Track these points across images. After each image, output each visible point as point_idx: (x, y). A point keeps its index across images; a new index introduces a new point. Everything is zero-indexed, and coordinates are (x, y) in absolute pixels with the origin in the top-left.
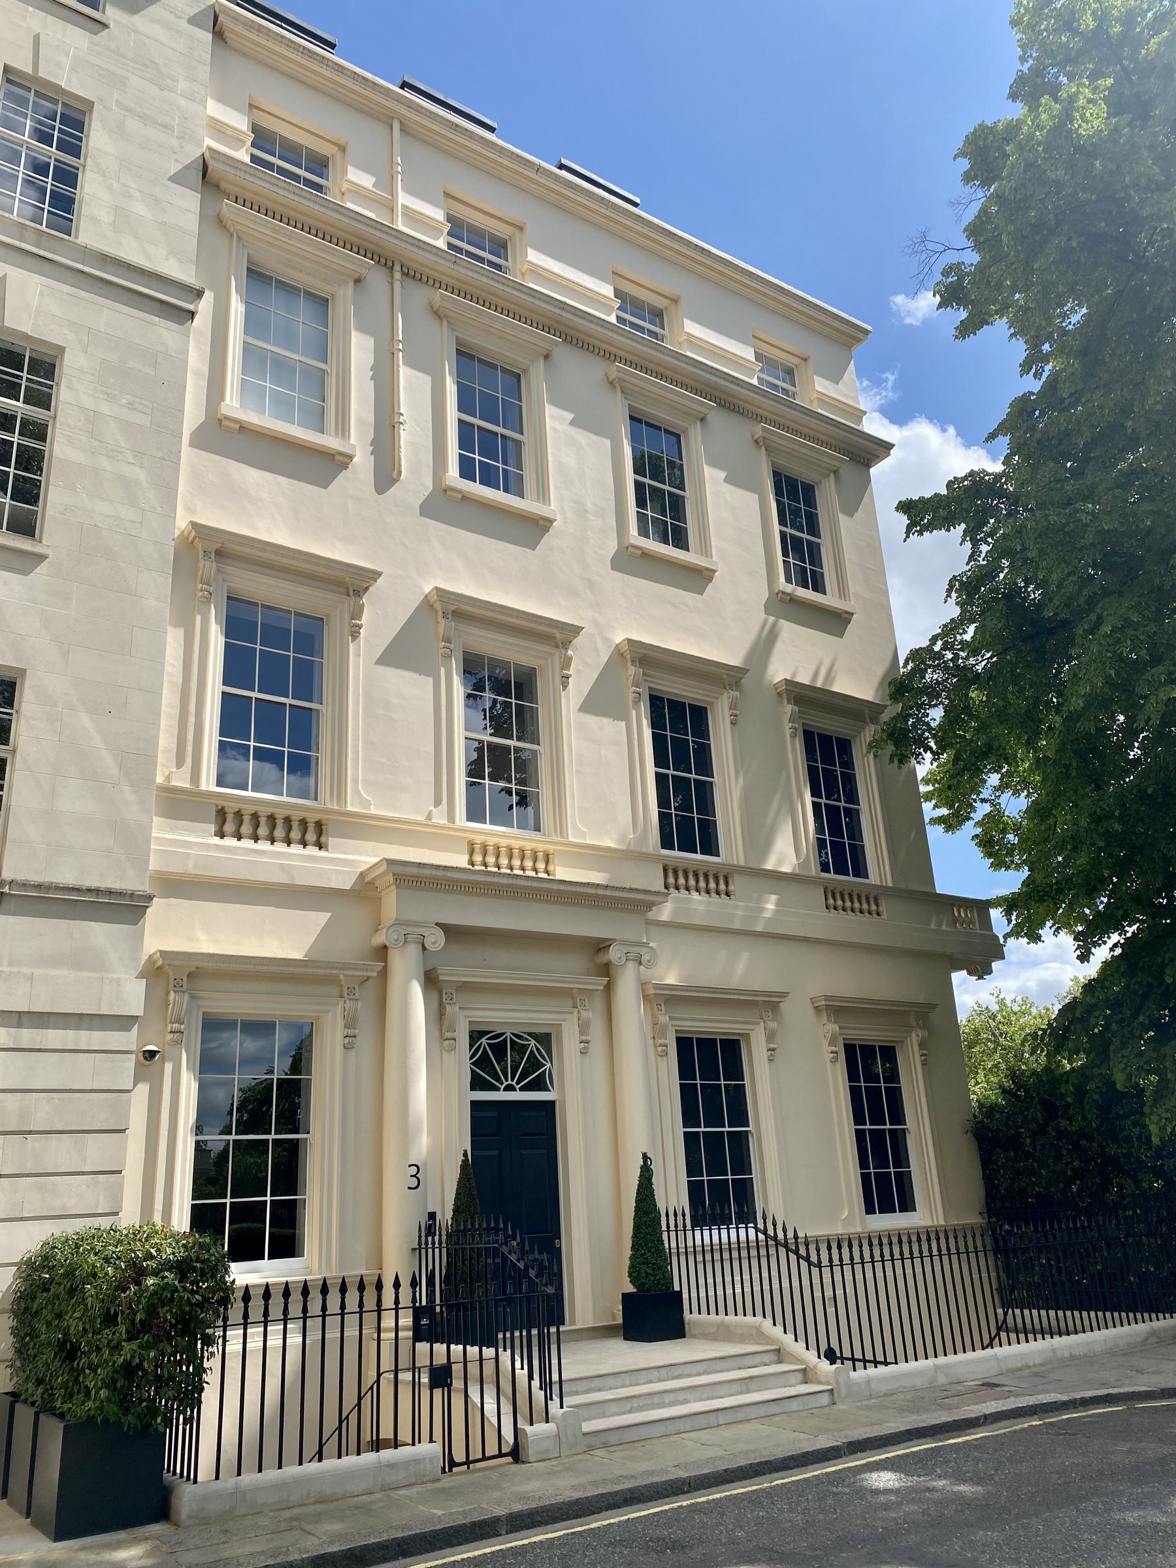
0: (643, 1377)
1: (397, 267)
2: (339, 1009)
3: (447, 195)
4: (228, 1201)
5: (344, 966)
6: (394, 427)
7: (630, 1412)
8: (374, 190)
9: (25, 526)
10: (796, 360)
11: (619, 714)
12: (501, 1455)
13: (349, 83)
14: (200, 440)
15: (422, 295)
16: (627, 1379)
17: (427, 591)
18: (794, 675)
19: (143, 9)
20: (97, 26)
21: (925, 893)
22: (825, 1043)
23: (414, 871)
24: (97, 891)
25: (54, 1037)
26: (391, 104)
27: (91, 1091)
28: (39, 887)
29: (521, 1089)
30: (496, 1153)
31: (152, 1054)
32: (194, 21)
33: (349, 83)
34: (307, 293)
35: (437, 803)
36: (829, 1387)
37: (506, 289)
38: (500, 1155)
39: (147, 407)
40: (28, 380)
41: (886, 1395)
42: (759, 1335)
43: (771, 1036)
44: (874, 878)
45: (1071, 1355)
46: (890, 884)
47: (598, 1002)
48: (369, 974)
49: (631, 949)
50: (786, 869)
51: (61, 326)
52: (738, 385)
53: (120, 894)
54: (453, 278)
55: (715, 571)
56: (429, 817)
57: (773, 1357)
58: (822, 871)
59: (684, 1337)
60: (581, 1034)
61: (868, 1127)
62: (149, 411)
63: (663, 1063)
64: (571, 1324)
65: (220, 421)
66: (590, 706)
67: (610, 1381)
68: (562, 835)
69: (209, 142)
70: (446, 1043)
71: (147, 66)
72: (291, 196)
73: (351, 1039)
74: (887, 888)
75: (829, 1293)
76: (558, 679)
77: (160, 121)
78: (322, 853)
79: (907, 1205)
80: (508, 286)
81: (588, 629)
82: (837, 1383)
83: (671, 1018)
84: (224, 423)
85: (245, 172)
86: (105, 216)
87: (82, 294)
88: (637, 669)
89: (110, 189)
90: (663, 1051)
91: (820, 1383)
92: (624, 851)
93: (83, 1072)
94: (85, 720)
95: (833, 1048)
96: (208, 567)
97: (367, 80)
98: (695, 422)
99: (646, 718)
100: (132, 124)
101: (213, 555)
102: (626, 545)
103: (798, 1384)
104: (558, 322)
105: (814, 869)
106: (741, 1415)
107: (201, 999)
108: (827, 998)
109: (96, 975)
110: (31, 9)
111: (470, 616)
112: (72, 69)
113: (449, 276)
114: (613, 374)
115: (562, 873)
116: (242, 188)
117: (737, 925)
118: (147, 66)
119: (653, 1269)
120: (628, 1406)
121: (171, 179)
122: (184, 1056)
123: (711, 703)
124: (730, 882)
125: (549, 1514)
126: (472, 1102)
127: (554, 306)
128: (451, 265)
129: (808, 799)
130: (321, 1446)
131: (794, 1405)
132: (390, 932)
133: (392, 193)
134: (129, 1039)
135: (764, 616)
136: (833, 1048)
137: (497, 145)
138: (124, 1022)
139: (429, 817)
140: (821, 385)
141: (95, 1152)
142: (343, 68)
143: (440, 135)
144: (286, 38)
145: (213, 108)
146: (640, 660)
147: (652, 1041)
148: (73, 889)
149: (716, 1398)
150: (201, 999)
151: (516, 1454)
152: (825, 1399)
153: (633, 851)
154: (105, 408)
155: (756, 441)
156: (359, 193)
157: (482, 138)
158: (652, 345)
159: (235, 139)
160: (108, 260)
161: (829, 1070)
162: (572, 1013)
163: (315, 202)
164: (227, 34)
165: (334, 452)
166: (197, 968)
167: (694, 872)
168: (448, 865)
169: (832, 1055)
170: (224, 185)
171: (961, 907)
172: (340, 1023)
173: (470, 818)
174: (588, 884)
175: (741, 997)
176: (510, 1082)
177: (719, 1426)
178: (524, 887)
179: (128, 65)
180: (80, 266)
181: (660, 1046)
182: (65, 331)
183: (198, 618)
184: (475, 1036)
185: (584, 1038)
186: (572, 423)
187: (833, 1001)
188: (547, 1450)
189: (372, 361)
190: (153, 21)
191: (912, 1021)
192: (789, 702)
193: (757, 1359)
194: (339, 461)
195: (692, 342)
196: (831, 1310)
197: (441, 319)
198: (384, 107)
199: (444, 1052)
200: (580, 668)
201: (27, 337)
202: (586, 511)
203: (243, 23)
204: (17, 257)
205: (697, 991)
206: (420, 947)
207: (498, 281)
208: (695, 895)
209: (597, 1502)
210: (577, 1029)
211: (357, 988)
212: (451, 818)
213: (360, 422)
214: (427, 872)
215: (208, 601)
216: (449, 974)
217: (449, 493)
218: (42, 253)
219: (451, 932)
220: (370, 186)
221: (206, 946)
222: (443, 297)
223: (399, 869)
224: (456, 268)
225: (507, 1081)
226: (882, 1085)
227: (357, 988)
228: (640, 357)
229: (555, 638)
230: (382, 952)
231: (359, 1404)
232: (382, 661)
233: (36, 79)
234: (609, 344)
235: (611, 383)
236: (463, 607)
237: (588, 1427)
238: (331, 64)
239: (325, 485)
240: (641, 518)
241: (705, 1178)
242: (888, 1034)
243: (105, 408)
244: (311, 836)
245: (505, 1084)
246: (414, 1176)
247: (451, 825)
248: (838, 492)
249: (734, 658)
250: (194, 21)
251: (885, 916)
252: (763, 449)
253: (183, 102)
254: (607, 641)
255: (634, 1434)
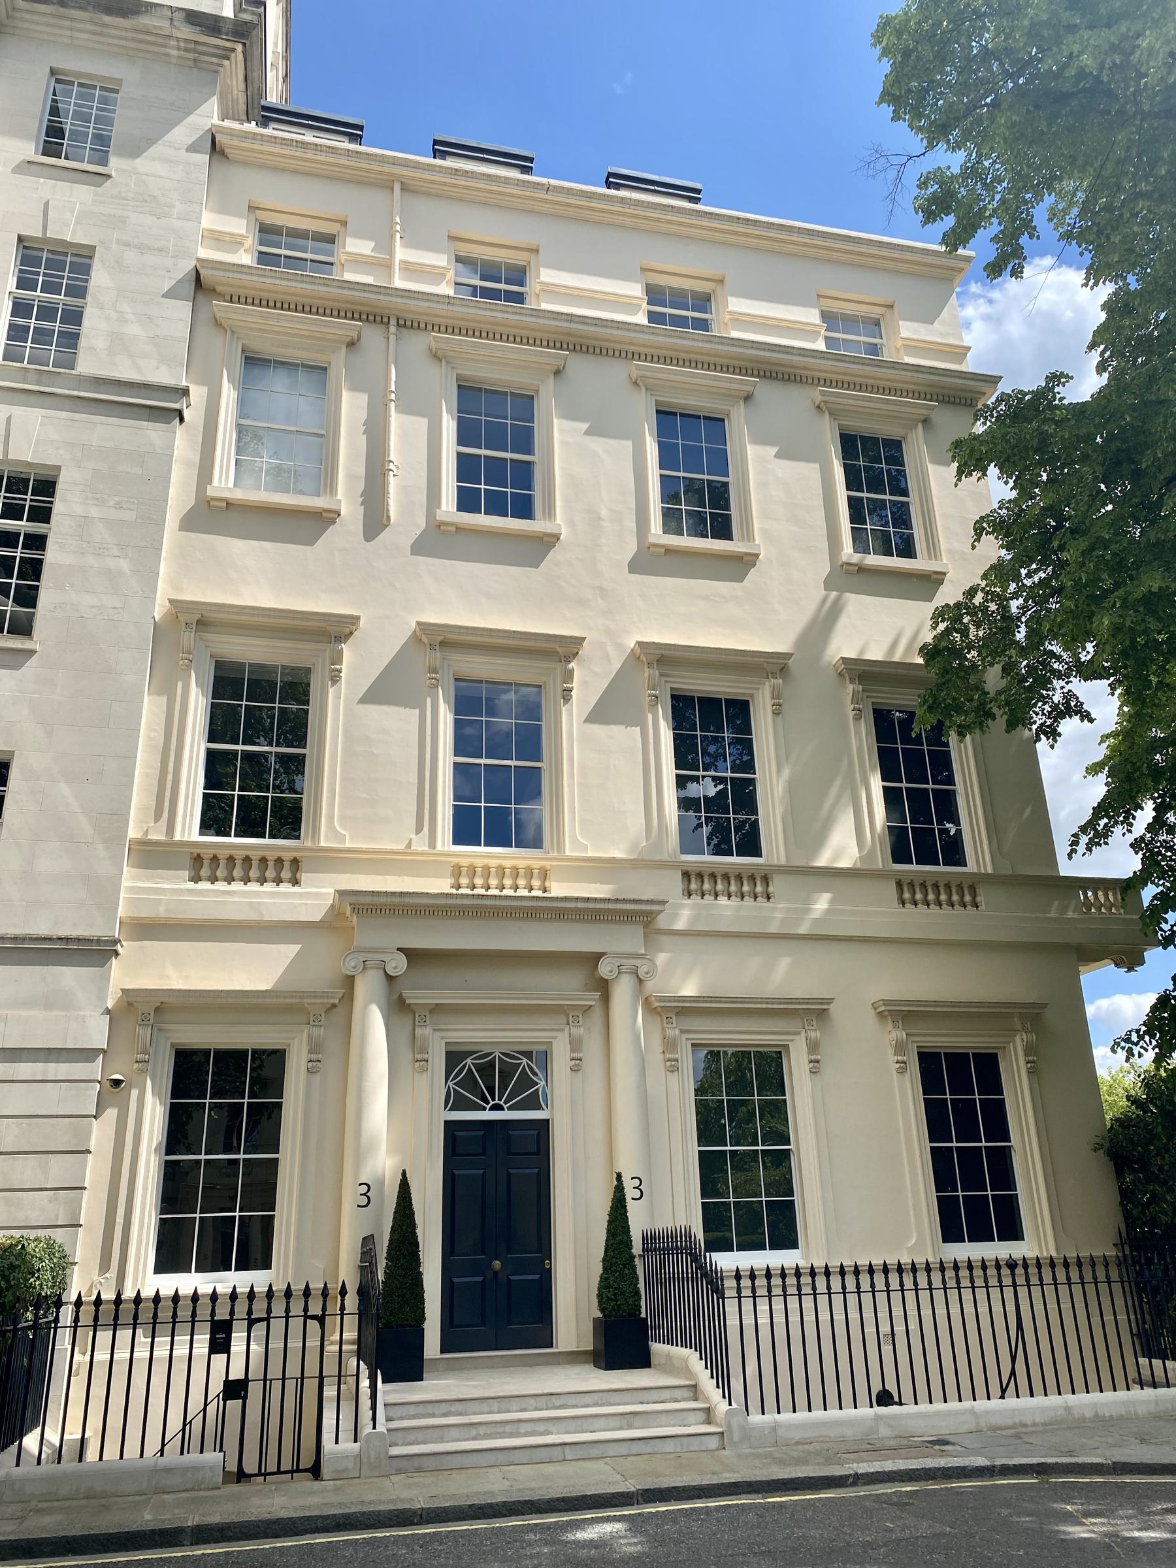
0: (514, 1404)
1: (393, 321)
2: (305, 1036)
3: (452, 238)
4: (237, 1214)
5: (315, 995)
6: (384, 473)
7: (474, 1439)
8: (373, 254)
9: (22, 628)
10: (880, 310)
11: (631, 718)
12: (279, 1472)
13: (343, 161)
14: (190, 523)
15: (418, 343)
16: (495, 1405)
17: (632, 646)
18: (862, 651)
19: (144, 152)
20: (104, 178)
21: (1047, 877)
22: (890, 1051)
23: (368, 900)
24: (67, 940)
25: (25, 1070)
26: (389, 169)
27: (57, 1116)
28: (15, 939)
29: (509, 1108)
30: (481, 1172)
31: (117, 1083)
32: (193, 148)
33: (343, 161)
34: (304, 366)
35: (419, 830)
36: (720, 1430)
37: (505, 316)
38: (484, 1174)
39: (133, 503)
40: (31, 500)
41: (797, 1443)
42: (686, 1370)
43: (813, 1046)
44: (971, 867)
45: (1096, 1415)
46: (990, 870)
47: (597, 1014)
48: (332, 1001)
49: (624, 961)
50: (845, 863)
51: (57, 449)
52: (787, 353)
53: (88, 941)
54: (450, 318)
55: (944, 574)
56: (409, 845)
57: (690, 1394)
58: (896, 860)
59: (649, 1366)
60: (572, 1051)
61: (984, 1144)
62: (135, 507)
63: (674, 1079)
64: (557, 1348)
65: (208, 502)
66: (598, 715)
67: (473, 1406)
68: (559, 850)
69: (204, 253)
70: (417, 1064)
71: (146, 201)
72: (278, 282)
73: (315, 1064)
74: (987, 876)
75: (885, 1329)
76: (559, 692)
77: (156, 247)
78: (296, 889)
79: (1012, 1231)
80: (507, 312)
81: (590, 636)
82: (729, 1426)
83: (682, 1032)
84: (212, 503)
85: (233, 272)
86: (101, 343)
87: (78, 416)
88: (856, 687)
89: (107, 319)
90: (671, 1066)
91: (717, 1425)
92: (631, 860)
93: (50, 1099)
94: (64, 789)
95: (899, 1058)
96: (189, 637)
97: (361, 153)
98: (916, 426)
99: (665, 719)
100: (131, 256)
101: (437, 647)
102: (647, 545)
103: (700, 1424)
104: (570, 335)
105: (882, 859)
106: (595, 1452)
107: (167, 1030)
108: (886, 1002)
109: (63, 1013)
110: (42, 180)
111: (456, 643)
112: (77, 223)
113: (446, 317)
114: (819, 398)
115: (558, 889)
116: (234, 286)
117: (773, 928)
118: (146, 201)
119: (615, 1295)
120: (474, 1432)
121: (165, 296)
122: (149, 1083)
123: (752, 696)
124: (770, 883)
125: (243, 1530)
126: (446, 1122)
127: (561, 320)
128: (445, 307)
129: (876, 784)
130: (163, 1445)
131: (669, 1446)
132: (348, 959)
133: (391, 252)
134: (95, 1069)
135: (823, 592)
136: (899, 1058)
137: (500, 177)
138: (87, 1055)
139: (409, 845)
140: (908, 330)
141: (58, 1170)
142: (336, 148)
143: (445, 184)
144: (279, 138)
145: (209, 220)
146: (859, 676)
147: (662, 1056)
148: (45, 939)
149: (586, 1432)
150: (167, 1030)
151: (315, 1471)
152: (713, 1443)
153: (643, 860)
154: (94, 512)
155: (818, 407)
156: (359, 262)
157: (483, 174)
158: (678, 334)
159: (235, 243)
160: (101, 381)
161: (896, 1084)
162: (563, 1030)
163: (302, 282)
164: (227, 150)
165: (320, 511)
166: (162, 1003)
167: (723, 875)
168: (403, 890)
169: (898, 1065)
170: (219, 288)
171: (1088, 888)
172: (305, 1049)
173: (458, 839)
174: (566, 898)
175: (770, 1006)
176: (497, 1101)
177: (565, 1460)
178: (492, 907)
179: (128, 205)
180: (75, 393)
181: (668, 1060)
182: (61, 452)
183: (180, 684)
184: (453, 1058)
185: (575, 1055)
186: (588, 433)
187: (981, 1007)
188: (346, 1470)
189: (365, 416)
190: (153, 159)
191: (1017, 1023)
192: (852, 681)
193: (666, 1394)
194: (327, 518)
195: (737, 320)
196: (887, 1349)
197: (441, 361)
198: (381, 173)
199: (416, 1074)
200: (587, 679)
201: (29, 464)
202: (600, 519)
203: (238, 136)
204: (22, 397)
205: (711, 1002)
206: (382, 972)
207: (496, 311)
208: (723, 900)
209: (302, 1524)
210: (568, 1046)
211: (323, 1015)
212: (432, 843)
213: (350, 477)
214: (383, 900)
215: (189, 668)
216: (414, 997)
217: (651, 549)
218: (42, 389)
219: (412, 955)
220: (369, 252)
221: (176, 982)
222: (436, 339)
223: (353, 899)
224: (450, 308)
225: (493, 1099)
226: (977, 1097)
227: (323, 1015)
228: (668, 349)
229: (558, 652)
230: (350, 981)
231: (205, 1410)
232: (364, 700)
233: (45, 240)
234: (630, 344)
235: (635, 383)
236: (450, 636)
237: (395, 1451)
238: (324, 149)
239: (311, 542)
240: (667, 514)
241: (764, 1199)
242: (974, 1039)
243: (94, 512)
244: (286, 874)
245: (492, 1103)
246: (364, 1194)
247: (431, 851)
248: (926, 442)
249: (781, 645)
250: (193, 148)
251: (983, 907)
252: (827, 414)
253: (178, 224)
254: (620, 647)
255: (456, 1461)
